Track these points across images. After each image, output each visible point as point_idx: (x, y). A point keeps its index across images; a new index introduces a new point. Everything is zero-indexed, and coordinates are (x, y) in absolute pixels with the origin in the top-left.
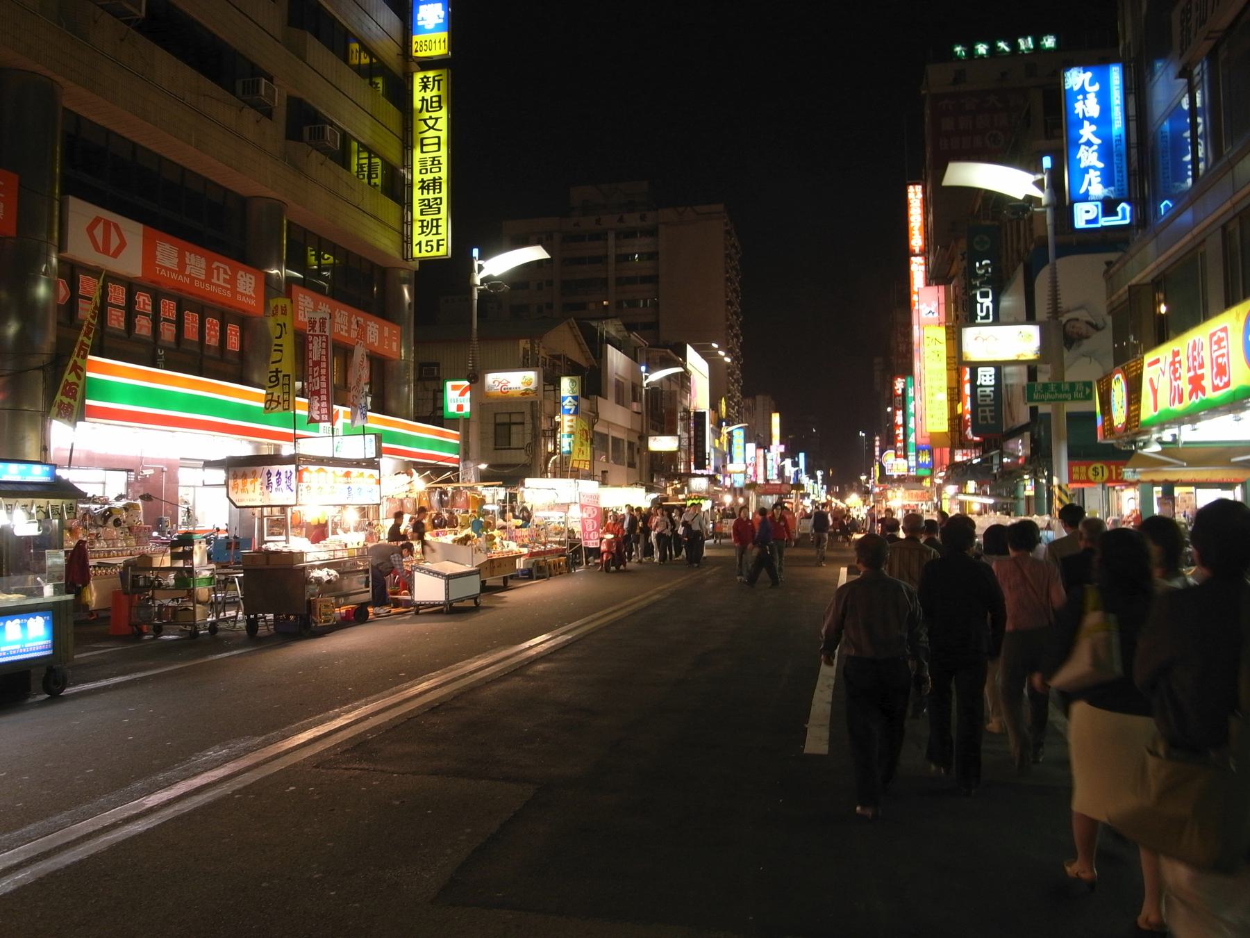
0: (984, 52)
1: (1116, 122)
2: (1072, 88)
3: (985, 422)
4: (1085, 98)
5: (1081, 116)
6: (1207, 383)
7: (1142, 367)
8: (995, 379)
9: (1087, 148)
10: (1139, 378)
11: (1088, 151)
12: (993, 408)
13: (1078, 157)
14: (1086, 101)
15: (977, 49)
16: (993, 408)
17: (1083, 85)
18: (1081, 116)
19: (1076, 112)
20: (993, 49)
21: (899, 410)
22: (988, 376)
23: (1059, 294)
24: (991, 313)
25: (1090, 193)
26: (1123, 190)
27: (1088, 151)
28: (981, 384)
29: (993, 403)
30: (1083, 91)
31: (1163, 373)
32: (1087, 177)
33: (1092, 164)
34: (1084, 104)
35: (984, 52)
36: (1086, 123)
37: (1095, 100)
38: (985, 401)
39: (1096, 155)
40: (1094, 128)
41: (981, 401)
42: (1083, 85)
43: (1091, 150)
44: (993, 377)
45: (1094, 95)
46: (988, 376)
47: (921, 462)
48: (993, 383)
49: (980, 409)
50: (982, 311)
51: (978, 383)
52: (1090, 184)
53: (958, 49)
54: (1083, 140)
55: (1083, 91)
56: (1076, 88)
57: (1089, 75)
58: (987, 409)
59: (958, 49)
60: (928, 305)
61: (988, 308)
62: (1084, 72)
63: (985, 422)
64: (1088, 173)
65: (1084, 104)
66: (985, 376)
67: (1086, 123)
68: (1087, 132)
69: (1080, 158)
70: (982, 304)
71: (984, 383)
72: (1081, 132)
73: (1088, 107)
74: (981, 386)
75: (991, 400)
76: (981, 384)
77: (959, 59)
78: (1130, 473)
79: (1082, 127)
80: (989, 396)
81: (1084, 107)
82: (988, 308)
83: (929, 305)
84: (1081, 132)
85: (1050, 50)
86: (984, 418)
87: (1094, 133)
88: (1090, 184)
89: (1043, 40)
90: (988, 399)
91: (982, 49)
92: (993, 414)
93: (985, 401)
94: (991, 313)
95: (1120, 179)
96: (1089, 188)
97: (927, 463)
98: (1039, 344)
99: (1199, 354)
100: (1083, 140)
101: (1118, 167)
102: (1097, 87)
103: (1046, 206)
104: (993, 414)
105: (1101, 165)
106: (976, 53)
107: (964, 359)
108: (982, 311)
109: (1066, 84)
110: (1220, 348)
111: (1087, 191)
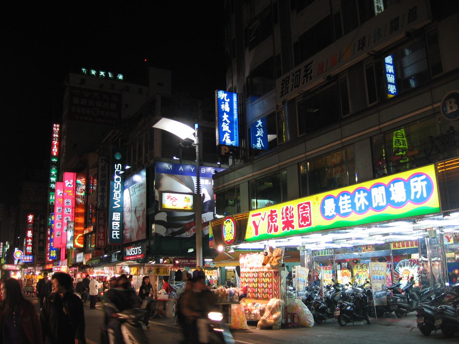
0: (94, 74)
1: (235, 116)
2: (220, 98)
3: (115, 238)
4: (224, 104)
5: (223, 110)
6: (296, 224)
7: (248, 216)
8: (120, 218)
9: (225, 124)
10: (246, 221)
11: (225, 125)
12: (119, 232)
13: (222, 126)
14: (225, 105)
15: (92, 72)
16: (119, 232)
17: (224, 98)
18: (223, 110)
19: (222, 108)
20: (98, 73)
21: (29, 231)
22: (117, 216)
23: (200, 183)
24: (120, 188)
25: (226, 142)
26: (237, 143)
27: (225, 125)
28: (114, 220)
29: (119, 229)
30: (223, 100)
31: (263, 219)
32: (225, 135)
33: (227, 130)
34: (224, 106)
35: (94, 74)
36: (225, 114)
37: (228, 105)
38: (116, 228)
39: (228, 127)
40: (227, 116)
41: (114, 228)
42: (224, 98)
43: (226, 125)
44: (119, 217)
45: (227, 103)
46: (117, 216)
47: (52, 256)
48: (119, 220)
49: (113, 232)
50: (116, 187)
51: (113, 220)
52: (226, 139)
53: (84, 70)
54: (224, 120)
55: (223, 100)
56: (222, 99)
57: (226, 95)
58: (116, 232)
59: (84, 70)
60: (68, 181)
61: (119, 185)
62: (225, 93)
63: (115, 238)
64: (225, 134)
65: (224, 106)
66: (116, 216)
67: (225, 114)
68: (225, 117)
69: (223, 127)
70: (116, 183)
71: (115, 220)
72: (223, 117)
73: (226, 107)
74: (114, 221)
75: (118, 228)
76: (114, 220)
77: (83, 74)
78: (212, 264)
79: (223, 115)
80: (117, 226)
81: (224, 107)
82: (119, 185)
83: (69, 181)
84: (223, 117)
85: (120, 80)
86: (115, 236)
87: (227, 118)
88: (226, 139)
89: (118, 76)
90: (117, 227)
91: (102, 73)
92: (119, 234)
93: (116, 228)
94: (120, 188)
95: (236, 138)
96: (226, 140)
97: (54, 256)
98: (193, 204)
99: (290, 212)
100: (224, 120)
101: (235, 134)
102: (228, 100)
103: (197, 144)
104: (119, 234)
105: (230, 131)
106: (91, 73)
107: (163, 207)
108: (116, 187)
109: (218, 96)
110: (304, 210)
111: (225, 141)
